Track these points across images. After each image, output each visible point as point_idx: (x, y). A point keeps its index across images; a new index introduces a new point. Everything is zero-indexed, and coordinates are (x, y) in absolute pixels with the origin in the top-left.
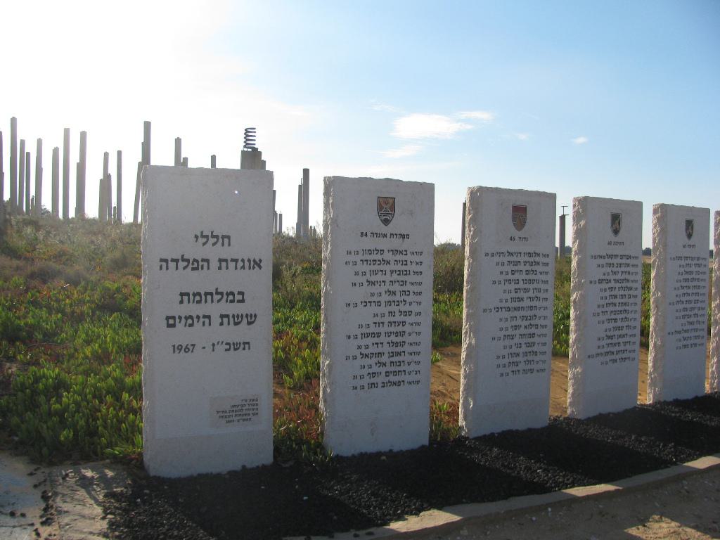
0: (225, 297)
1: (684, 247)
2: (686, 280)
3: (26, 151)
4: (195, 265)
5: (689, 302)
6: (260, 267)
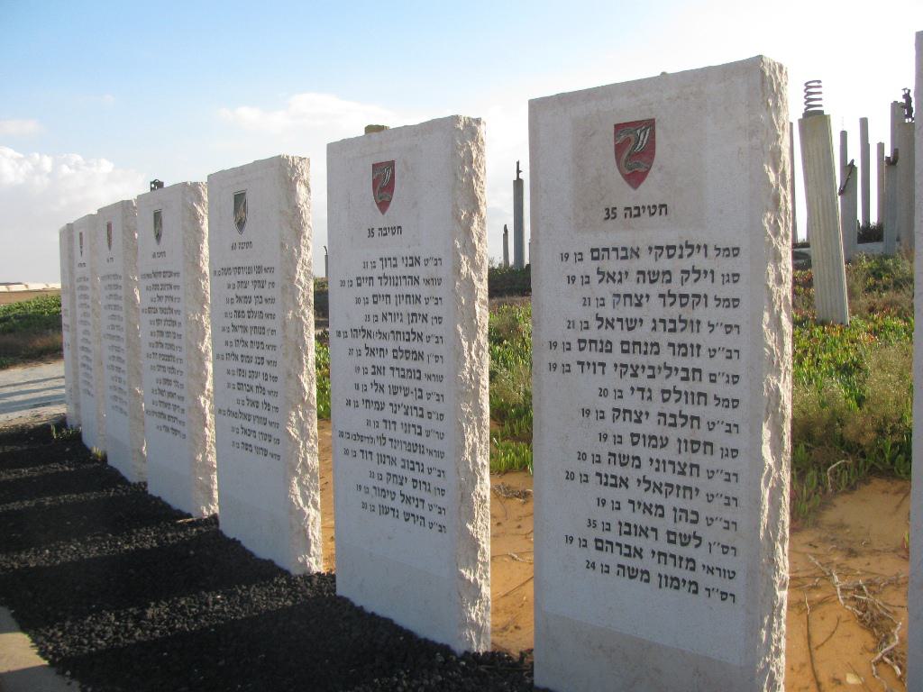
0: (678, 300)
1: (233, 247)
2: (239, 314)
5: (248, 359)
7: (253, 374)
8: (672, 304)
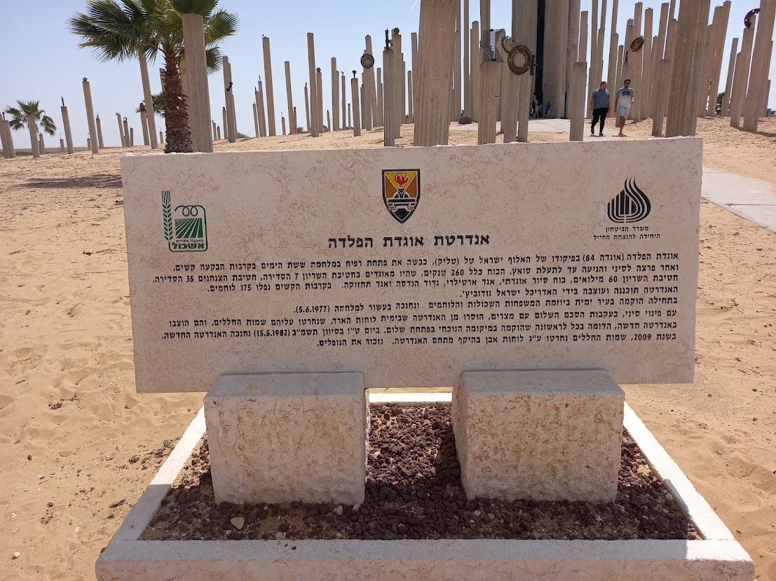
0: (331, 264)
3: (294, 106)
4: (360, 243)
6: (488, 242)
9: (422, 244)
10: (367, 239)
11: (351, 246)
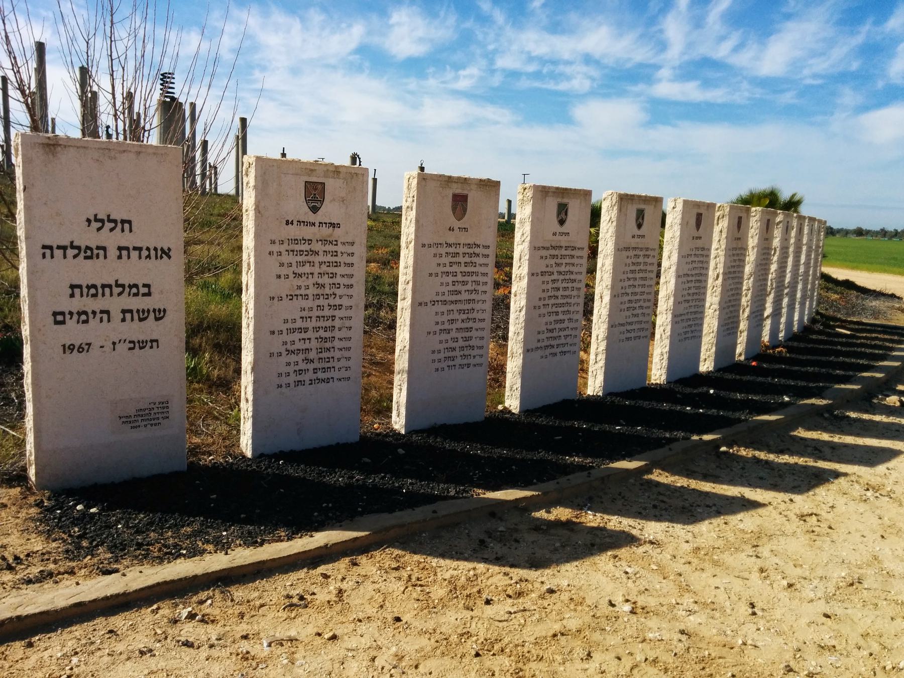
0: (127, 290)
7: (637, 301)
8: (120, 294)
9: (169, 257)
10: (98, 248)
11: (75, 257)
